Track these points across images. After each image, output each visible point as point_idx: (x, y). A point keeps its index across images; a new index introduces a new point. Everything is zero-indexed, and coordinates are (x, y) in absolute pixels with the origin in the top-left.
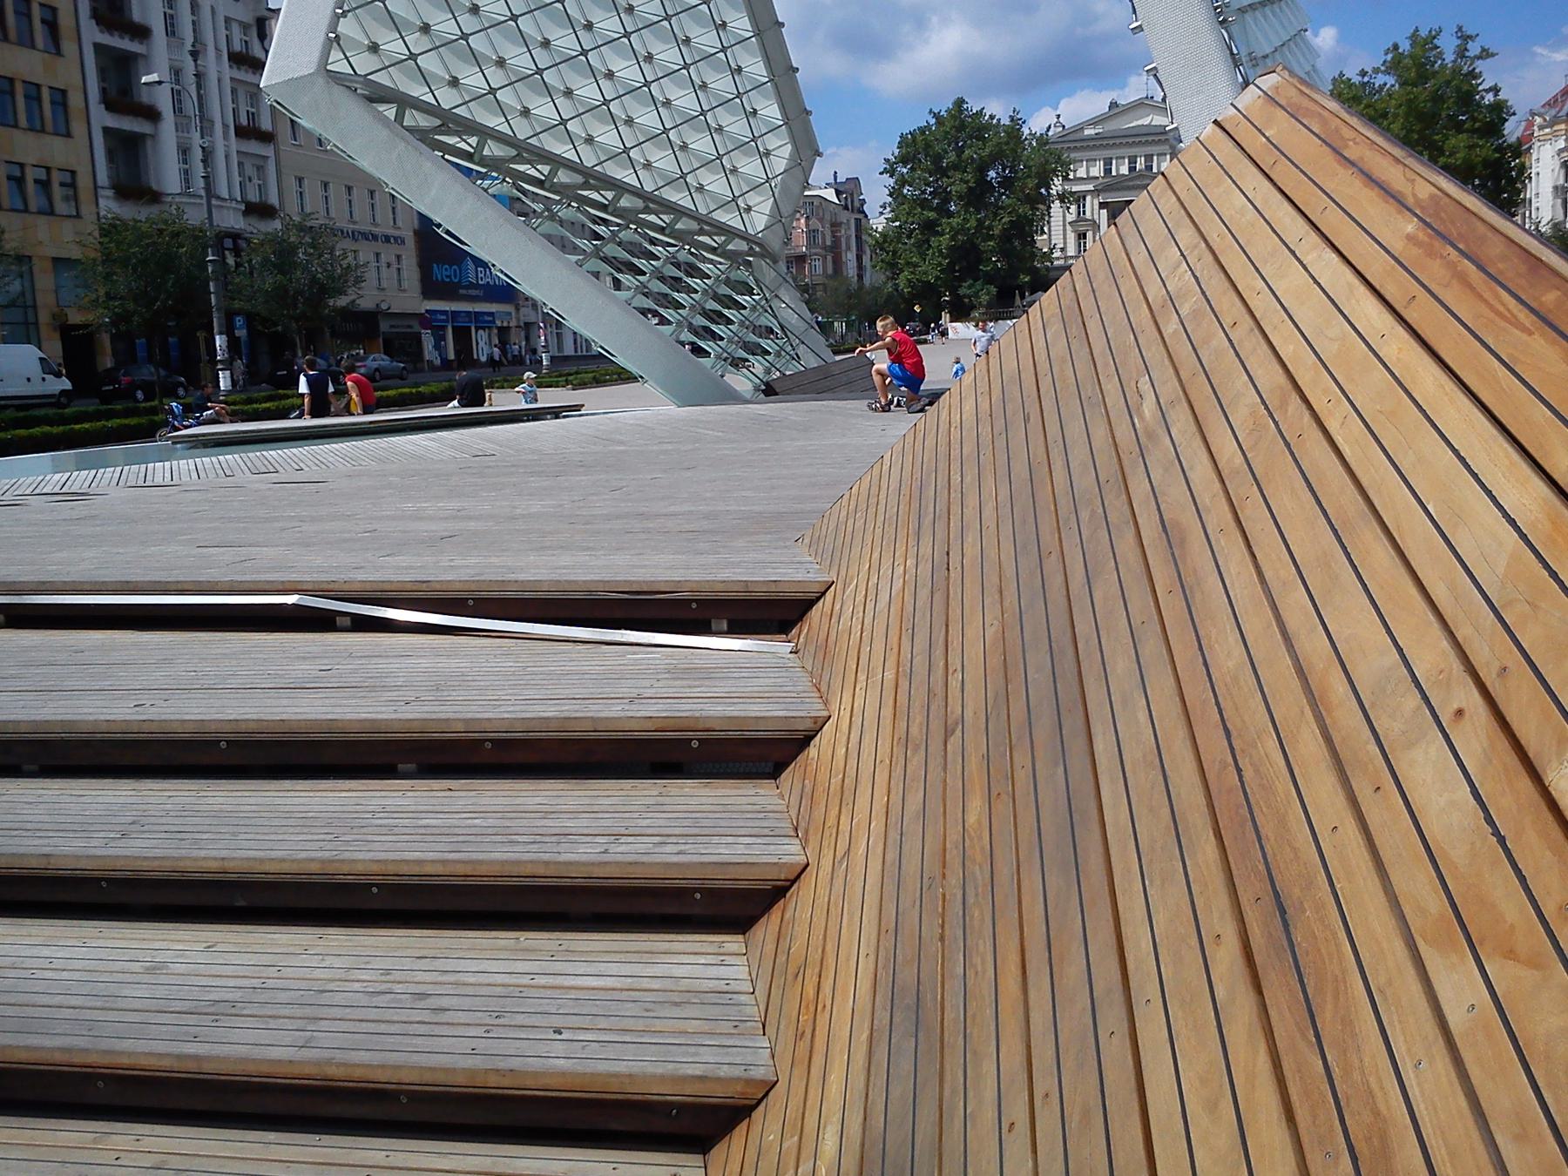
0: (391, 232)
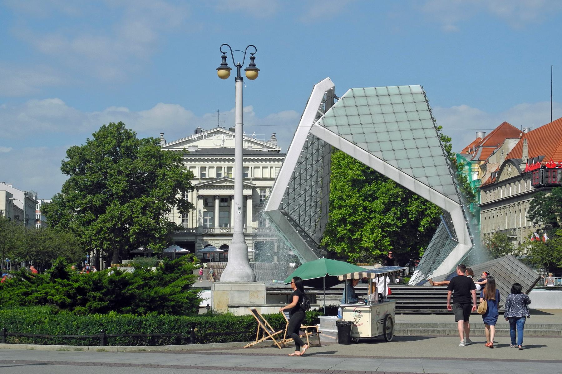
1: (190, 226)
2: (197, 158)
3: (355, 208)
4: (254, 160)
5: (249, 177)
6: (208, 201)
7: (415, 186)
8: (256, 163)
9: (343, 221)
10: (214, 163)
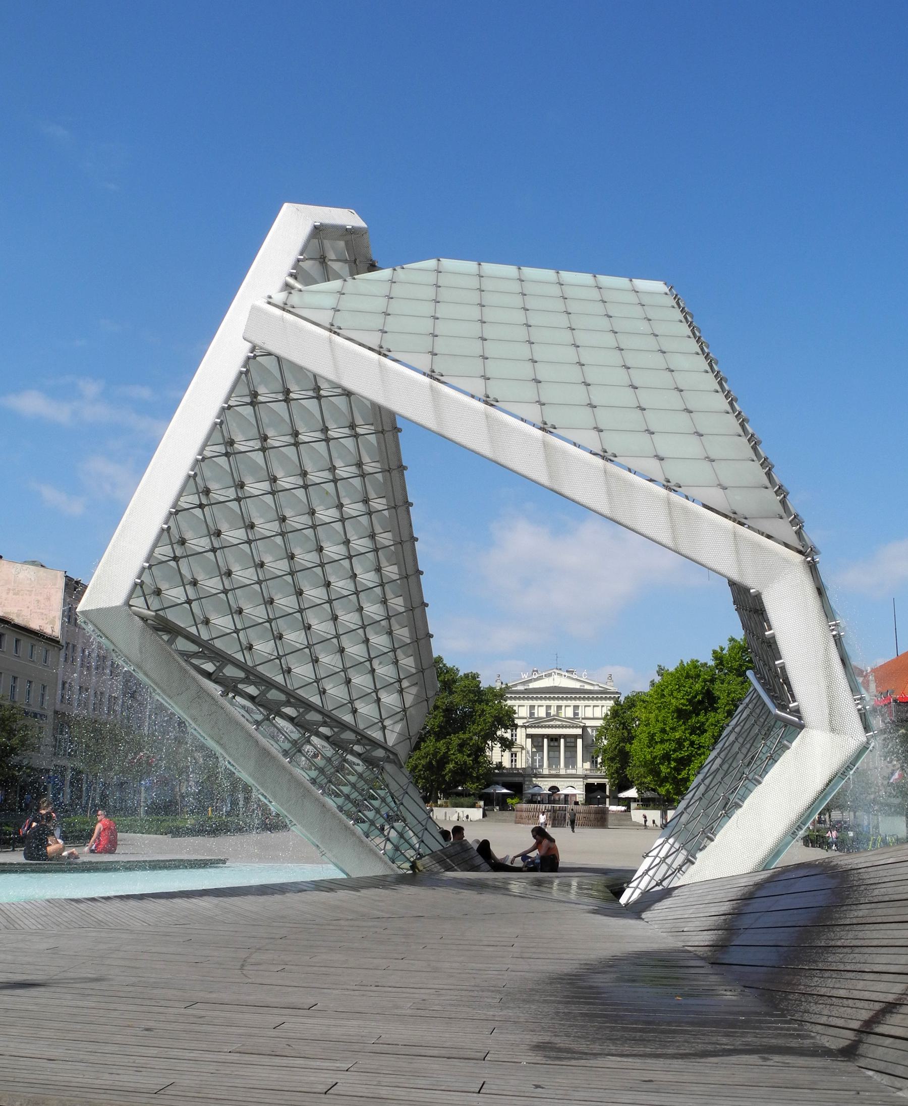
0: (37, 710)
1: (519, 766)
2: (526, 696)
3: (680, 743)
4: (584, 699)
5: (580, 716)
6: (536, 740)
7: (609, 493)
8: (586, 702)
9: (666, 757)
10: (544, 702)
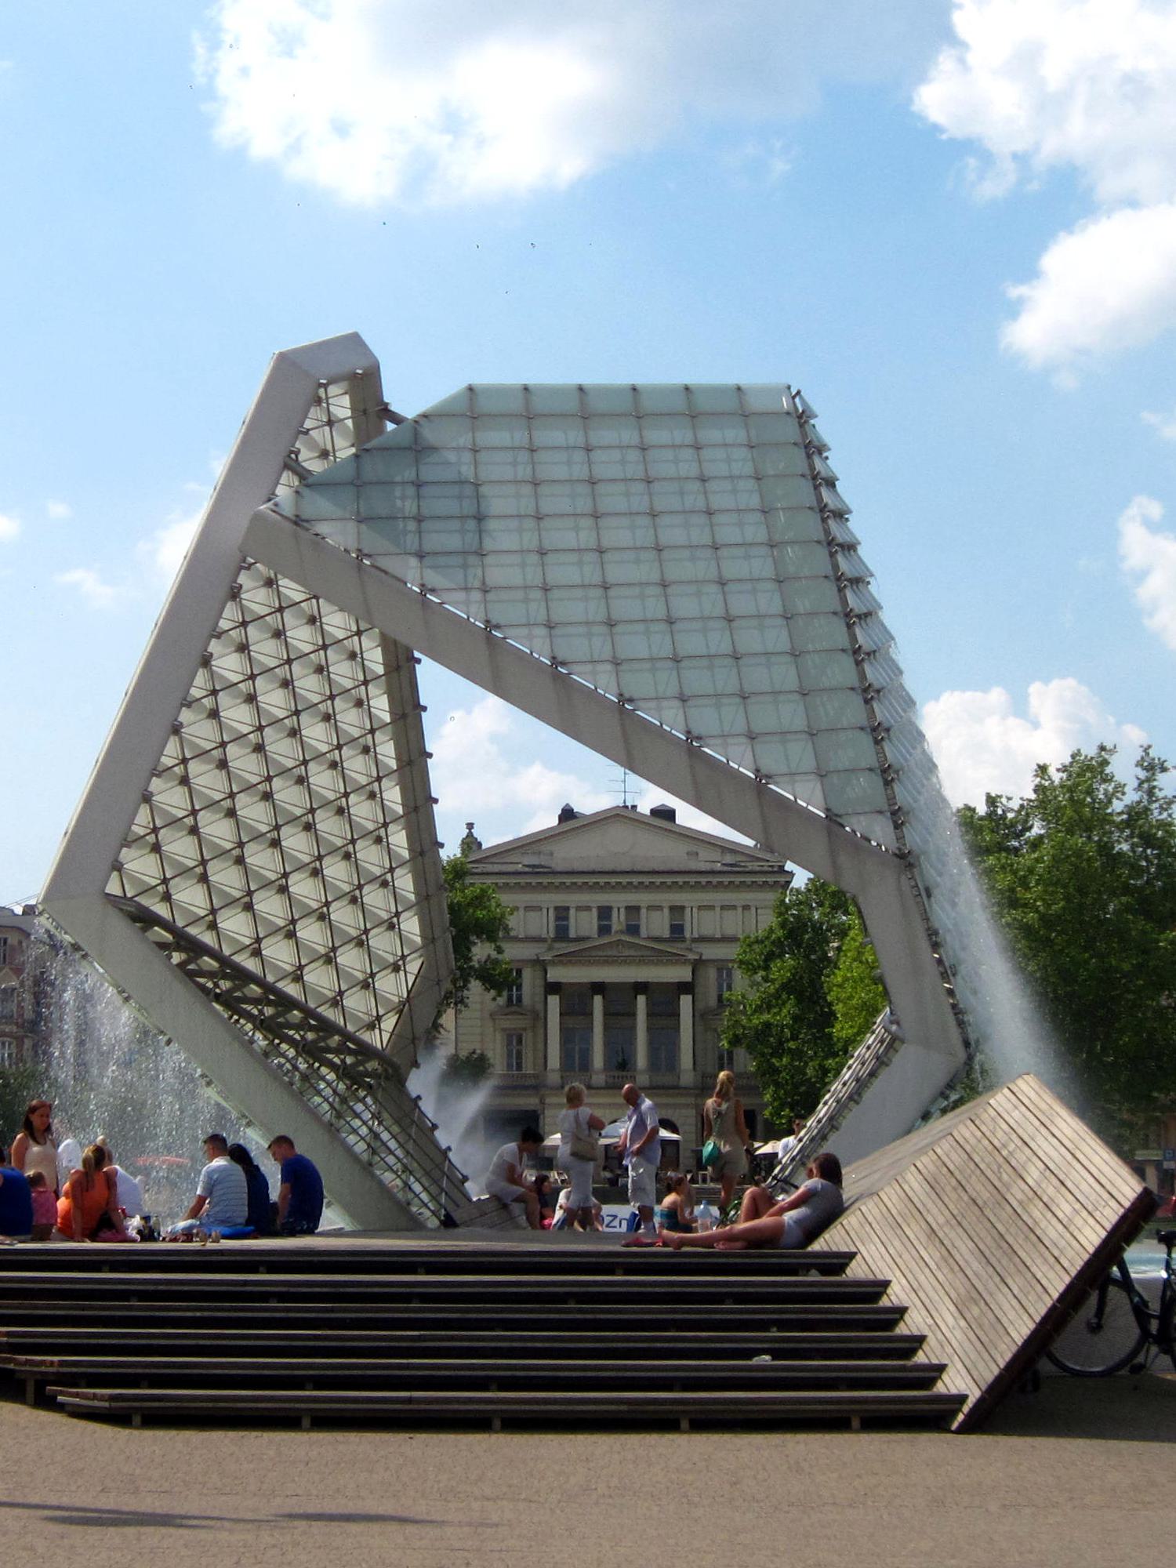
5: (688, 934)
